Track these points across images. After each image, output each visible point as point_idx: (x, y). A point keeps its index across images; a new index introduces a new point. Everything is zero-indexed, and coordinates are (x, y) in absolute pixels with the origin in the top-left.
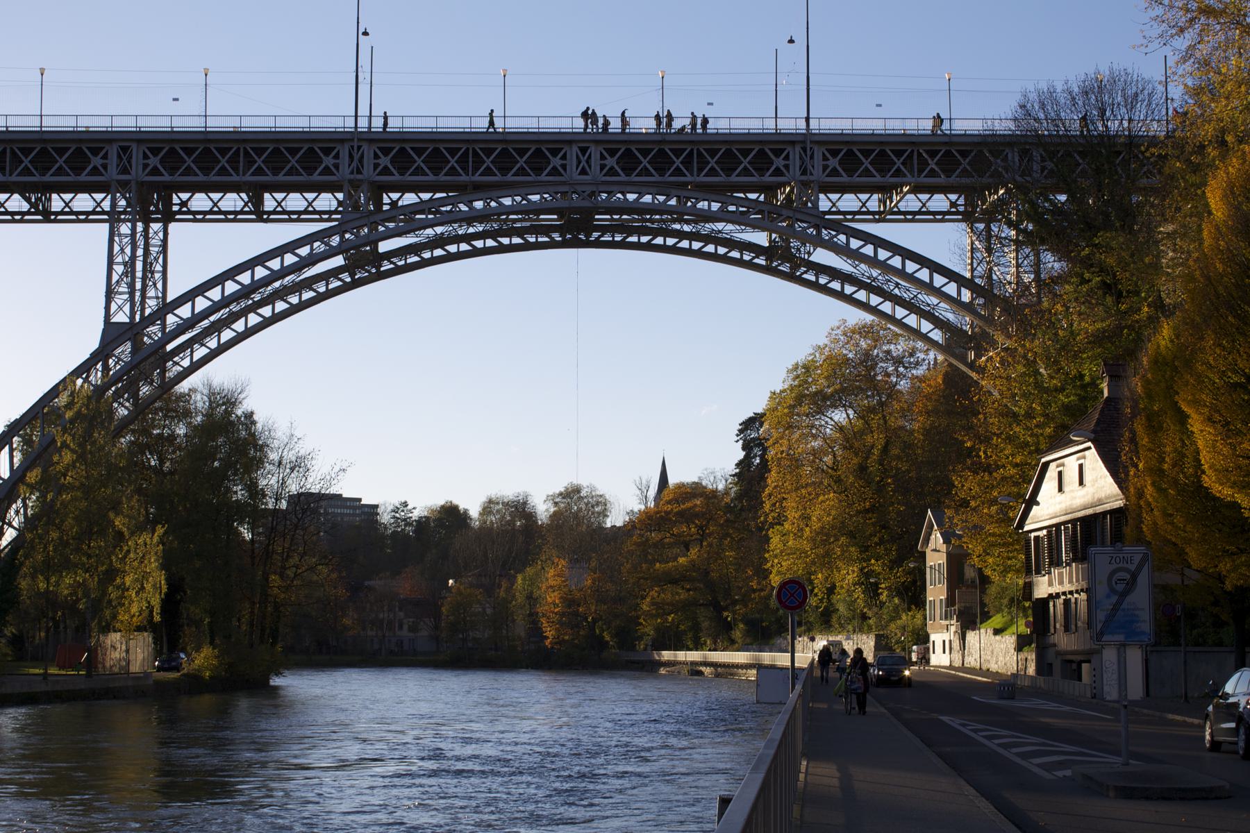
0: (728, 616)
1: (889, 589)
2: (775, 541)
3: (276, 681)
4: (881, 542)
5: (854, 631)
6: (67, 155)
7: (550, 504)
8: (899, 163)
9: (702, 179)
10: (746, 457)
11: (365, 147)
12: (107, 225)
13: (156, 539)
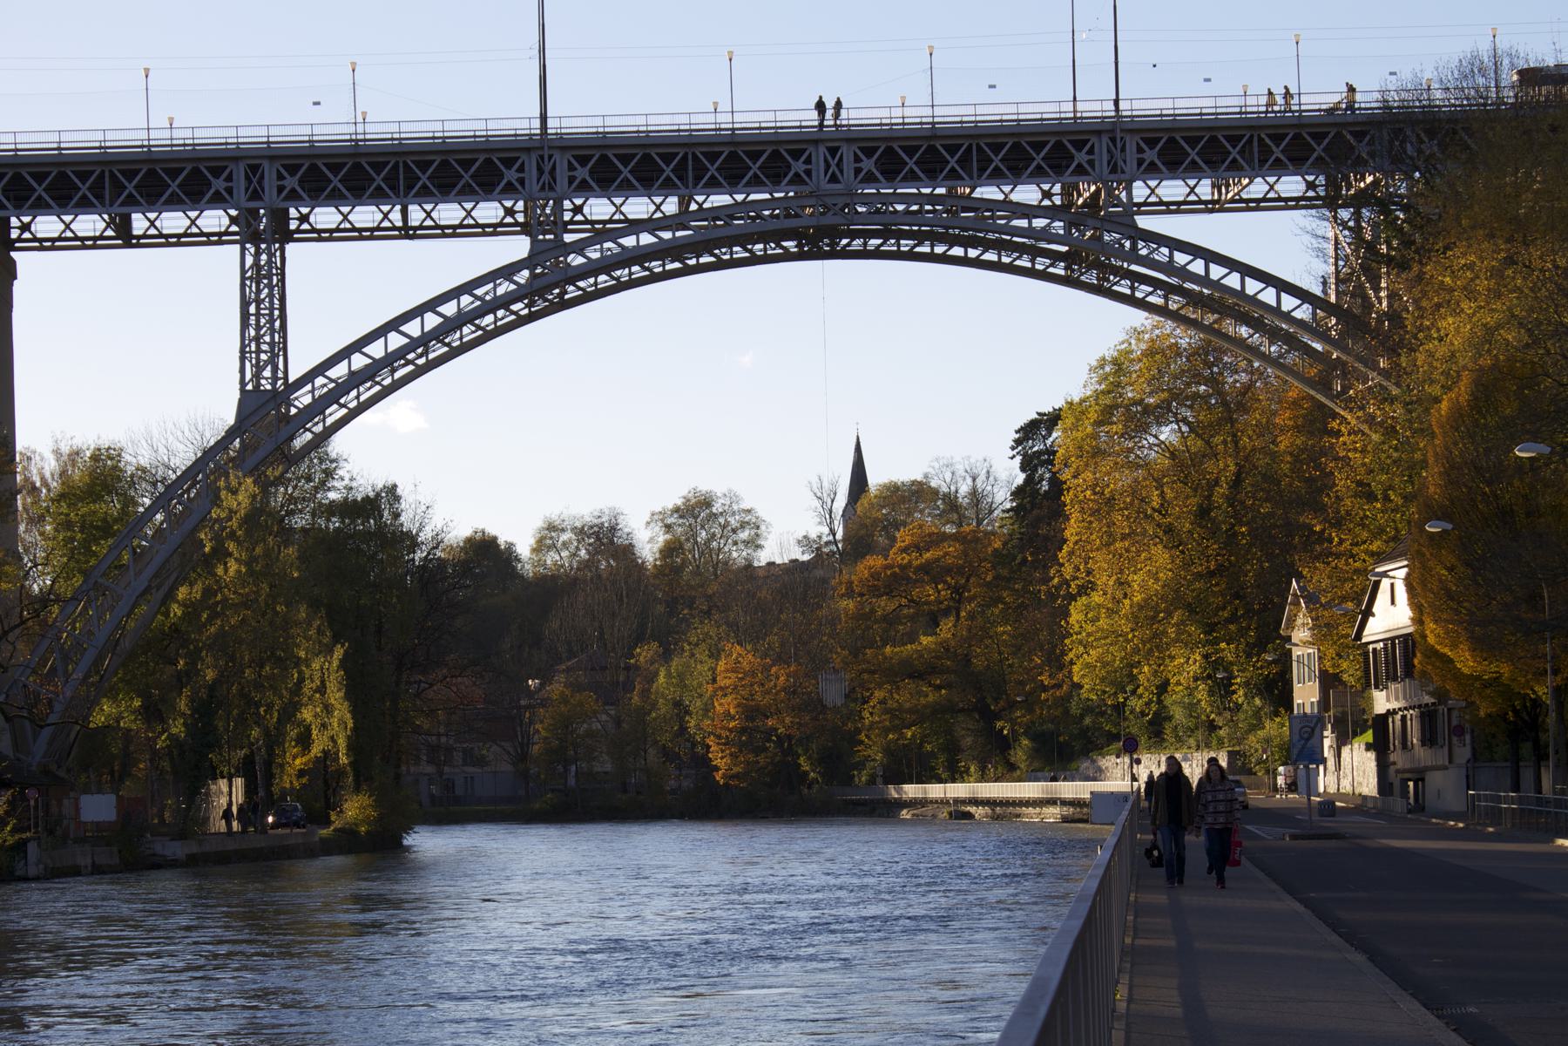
1: (1247, 684)
4: (1233, 619)
6: (181, 178)
7: (657, 529)
8: (1234, 153)
10: (1028, 481)
11: (557, 156)
12: (237, 247)
13: (335, 664)
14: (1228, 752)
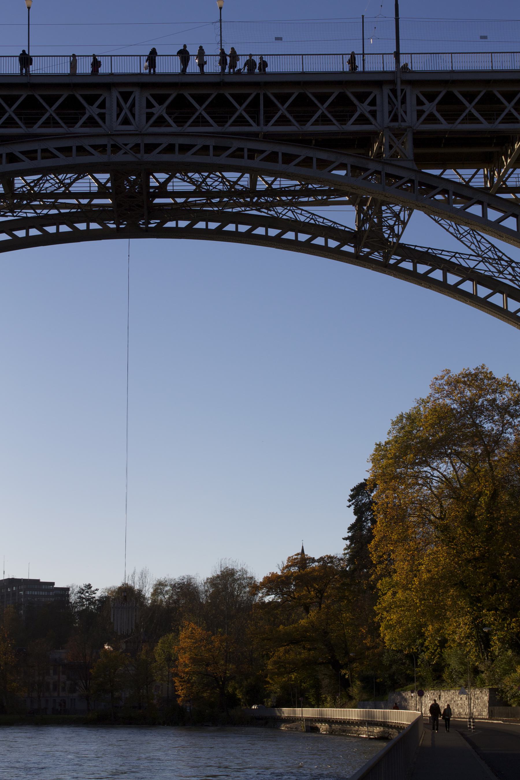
0: (345, 674)
5: (466, 686)
9: (271, 128)
14: (490, 689)
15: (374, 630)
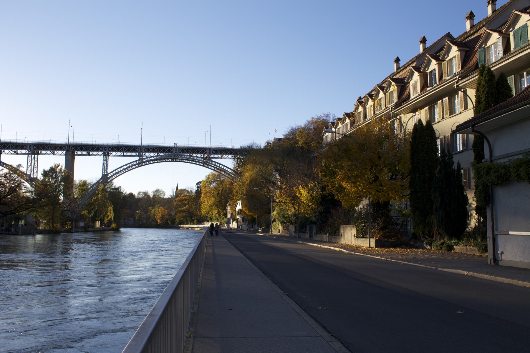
2: (202, 205)
3: (120, 230)
15: (200, 211)
